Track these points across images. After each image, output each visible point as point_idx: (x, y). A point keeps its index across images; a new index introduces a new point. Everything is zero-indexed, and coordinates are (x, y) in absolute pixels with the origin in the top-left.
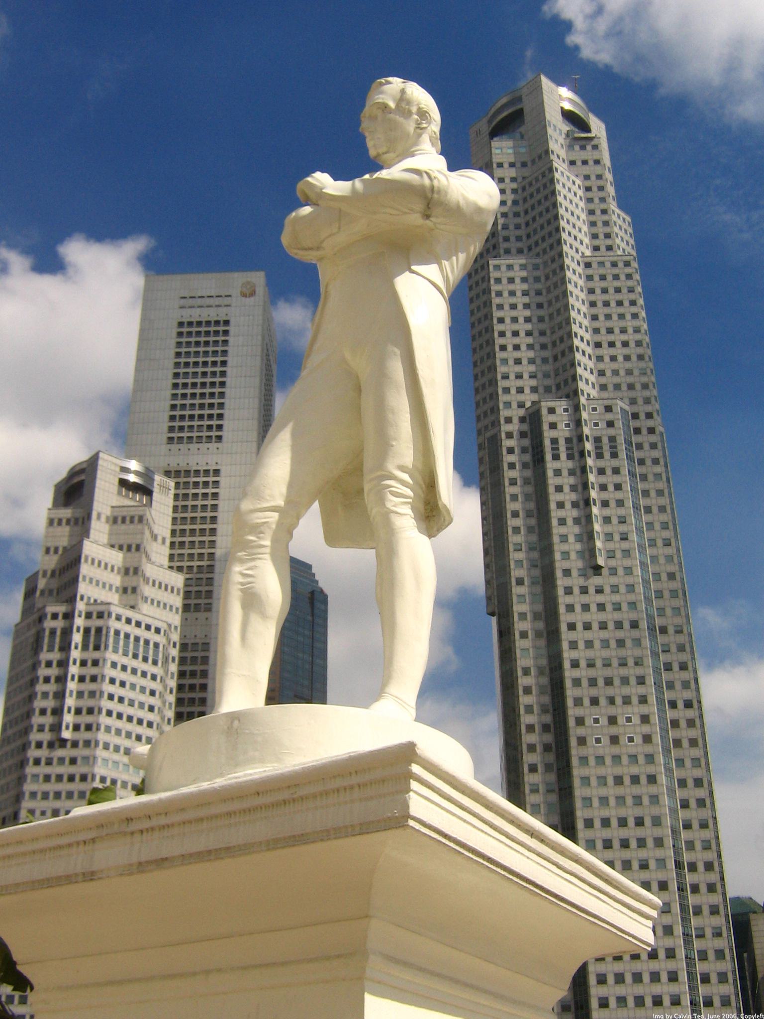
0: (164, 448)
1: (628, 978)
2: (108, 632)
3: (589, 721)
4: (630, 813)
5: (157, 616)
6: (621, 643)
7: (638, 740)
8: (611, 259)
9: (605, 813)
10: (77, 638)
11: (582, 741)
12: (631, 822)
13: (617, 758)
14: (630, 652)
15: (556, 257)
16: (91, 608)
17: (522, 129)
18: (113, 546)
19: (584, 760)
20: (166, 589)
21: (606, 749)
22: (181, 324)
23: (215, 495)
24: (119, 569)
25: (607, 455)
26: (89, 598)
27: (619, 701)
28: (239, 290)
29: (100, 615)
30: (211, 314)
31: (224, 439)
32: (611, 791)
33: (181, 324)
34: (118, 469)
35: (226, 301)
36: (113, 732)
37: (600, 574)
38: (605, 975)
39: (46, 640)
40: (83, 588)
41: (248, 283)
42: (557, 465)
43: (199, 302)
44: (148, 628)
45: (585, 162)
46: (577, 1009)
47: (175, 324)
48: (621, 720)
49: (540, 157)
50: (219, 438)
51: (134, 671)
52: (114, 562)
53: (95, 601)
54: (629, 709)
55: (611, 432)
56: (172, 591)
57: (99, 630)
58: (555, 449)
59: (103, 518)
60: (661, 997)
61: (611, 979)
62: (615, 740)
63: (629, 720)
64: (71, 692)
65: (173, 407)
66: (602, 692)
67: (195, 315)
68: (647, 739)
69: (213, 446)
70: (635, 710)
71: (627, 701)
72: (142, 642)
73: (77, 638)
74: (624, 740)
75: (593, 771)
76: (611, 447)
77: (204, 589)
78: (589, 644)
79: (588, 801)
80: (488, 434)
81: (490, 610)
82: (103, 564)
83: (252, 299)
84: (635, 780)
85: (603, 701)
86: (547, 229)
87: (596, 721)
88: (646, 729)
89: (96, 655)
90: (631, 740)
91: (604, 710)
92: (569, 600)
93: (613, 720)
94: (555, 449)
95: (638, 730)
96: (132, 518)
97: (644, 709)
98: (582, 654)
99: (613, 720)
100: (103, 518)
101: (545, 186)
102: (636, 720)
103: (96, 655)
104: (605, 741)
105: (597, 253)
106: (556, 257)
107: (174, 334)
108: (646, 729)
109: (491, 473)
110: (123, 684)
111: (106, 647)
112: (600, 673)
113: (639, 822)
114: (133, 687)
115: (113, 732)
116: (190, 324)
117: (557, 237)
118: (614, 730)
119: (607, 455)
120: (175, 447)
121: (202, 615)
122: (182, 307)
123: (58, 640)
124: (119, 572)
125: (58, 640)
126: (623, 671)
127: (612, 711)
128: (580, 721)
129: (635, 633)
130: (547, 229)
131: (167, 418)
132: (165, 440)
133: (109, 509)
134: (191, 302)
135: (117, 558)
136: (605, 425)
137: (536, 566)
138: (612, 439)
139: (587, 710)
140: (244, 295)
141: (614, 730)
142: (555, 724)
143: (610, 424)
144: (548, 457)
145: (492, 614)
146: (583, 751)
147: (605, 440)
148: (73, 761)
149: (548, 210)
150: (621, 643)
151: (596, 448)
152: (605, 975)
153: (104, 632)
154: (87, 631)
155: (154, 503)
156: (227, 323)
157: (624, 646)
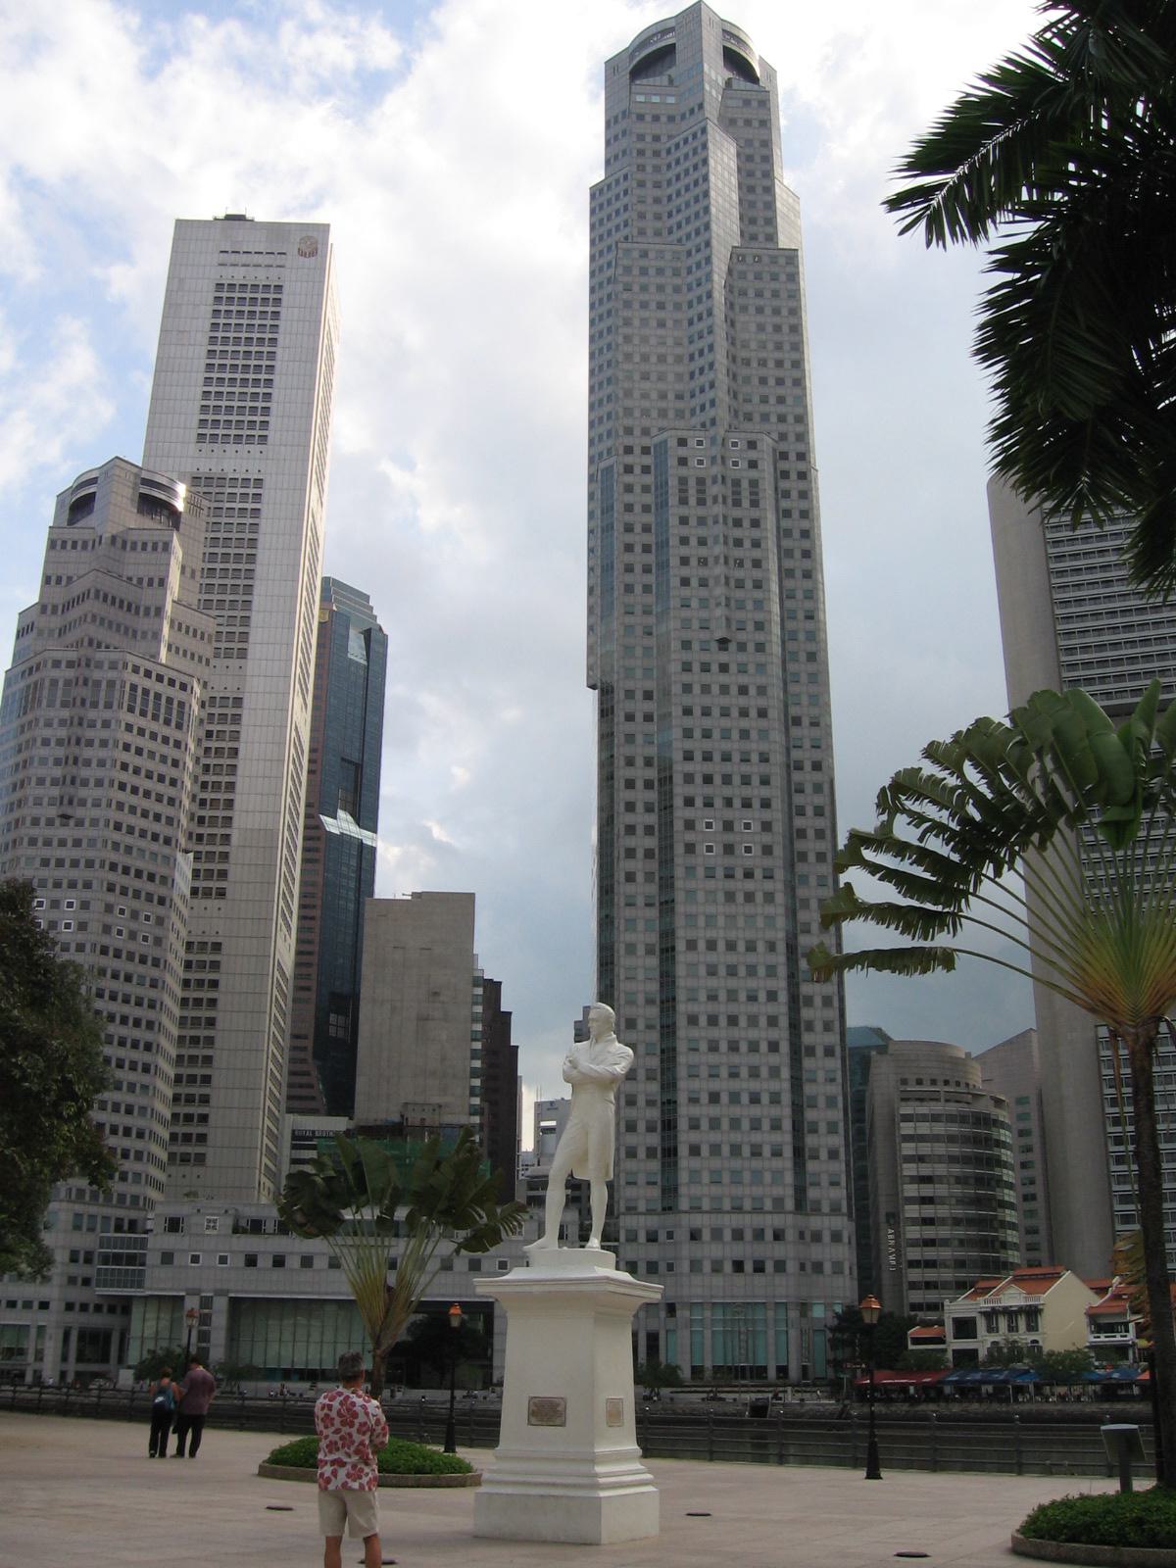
0: (193, 448)
1: (725, 1124)
2: (123, 686)
3: (701, 826)
5: (183, 669)
6: (745, 734)
7: (757, 850)
8: (771, 252)
9: (711, 934)
11: (690, 848)
14: (754, 746)
15: (703, 246)
17: (673, 72)
19: (690, 870)
20: (195, 635)
22: (219, 286)
27: (737, 803)
28: (296, 247)
30: (261, 277)
31: (270, 440)
33: (219, 286)
35: (280, 260)
36: (126, 809)
37: (726, 649)
38: (698, 1120)
39: (45, 693)
41: (309, 238)
42: (684, 511)
43: (244, 259)
44: (172, 682)
45: (748, 122)
46: (663, 1129)
47: (212, 287)
49: (692, 111)
50: (263, 439)
51: (154, 736)
54: (747, 812)
55: (754, 474)
56: (202, 638)
58: (683, 491)
60: (758, 1094)
61: (705, 1124)
66: (718, 791)
67: (238, 275)
68: (767, 850)
69: (255, 448)
70: (756, 814)
71: (747, 804)
72: (163, 701)
74: (740, 850)
76: (751, 494)
77: (238, 630)
78: (706, 689)
79: (691, 918)
80: (603, 465)
81: (592, 682)
84: (754, 1047)
86: (694, 208)
88: (767, 838)
90: (748, 850)
91: (720, 812)
93: (728, 826)
94: (683, 491)
95: (757, 838)
97: (767, 815)
98: (724, 1033)
99: (728, 826)
101: (695, 152)
102: (756, 827)
104: (718, 849)
106: (703, 246)
107: (211, 300)
108: (767, 838)
109: (602, 513)
110: (139, 751)
111: (120, 706)
112: (716, 768)
114: (152, 755)
115: (126, 809)
117: (704, 172)
118: (729, 838)
121: (234, 663)
123: (60, 693)
125: (60, 693)
126: (745, 768)
128: (690, 825)
129: (762, 723)
130: (694, 208)
131: (197, 409)
132: (194, 437)
134: (233, 258)
136: (746, 465)
138: (754, 484)
139: (696, 813)
140: (302, 253)
141: (729, 838)
142: (660, 825)
143: (753, 464)
144: (673, 500)
145: (593, 687)
146: (691, 860)
147: (745, 484)
148: (77, 843)
149: (696, 183)
150: (745, 734)
151: (734, 493)
152: (698, 1120)
153: (118, 686)
156: (279, 288)
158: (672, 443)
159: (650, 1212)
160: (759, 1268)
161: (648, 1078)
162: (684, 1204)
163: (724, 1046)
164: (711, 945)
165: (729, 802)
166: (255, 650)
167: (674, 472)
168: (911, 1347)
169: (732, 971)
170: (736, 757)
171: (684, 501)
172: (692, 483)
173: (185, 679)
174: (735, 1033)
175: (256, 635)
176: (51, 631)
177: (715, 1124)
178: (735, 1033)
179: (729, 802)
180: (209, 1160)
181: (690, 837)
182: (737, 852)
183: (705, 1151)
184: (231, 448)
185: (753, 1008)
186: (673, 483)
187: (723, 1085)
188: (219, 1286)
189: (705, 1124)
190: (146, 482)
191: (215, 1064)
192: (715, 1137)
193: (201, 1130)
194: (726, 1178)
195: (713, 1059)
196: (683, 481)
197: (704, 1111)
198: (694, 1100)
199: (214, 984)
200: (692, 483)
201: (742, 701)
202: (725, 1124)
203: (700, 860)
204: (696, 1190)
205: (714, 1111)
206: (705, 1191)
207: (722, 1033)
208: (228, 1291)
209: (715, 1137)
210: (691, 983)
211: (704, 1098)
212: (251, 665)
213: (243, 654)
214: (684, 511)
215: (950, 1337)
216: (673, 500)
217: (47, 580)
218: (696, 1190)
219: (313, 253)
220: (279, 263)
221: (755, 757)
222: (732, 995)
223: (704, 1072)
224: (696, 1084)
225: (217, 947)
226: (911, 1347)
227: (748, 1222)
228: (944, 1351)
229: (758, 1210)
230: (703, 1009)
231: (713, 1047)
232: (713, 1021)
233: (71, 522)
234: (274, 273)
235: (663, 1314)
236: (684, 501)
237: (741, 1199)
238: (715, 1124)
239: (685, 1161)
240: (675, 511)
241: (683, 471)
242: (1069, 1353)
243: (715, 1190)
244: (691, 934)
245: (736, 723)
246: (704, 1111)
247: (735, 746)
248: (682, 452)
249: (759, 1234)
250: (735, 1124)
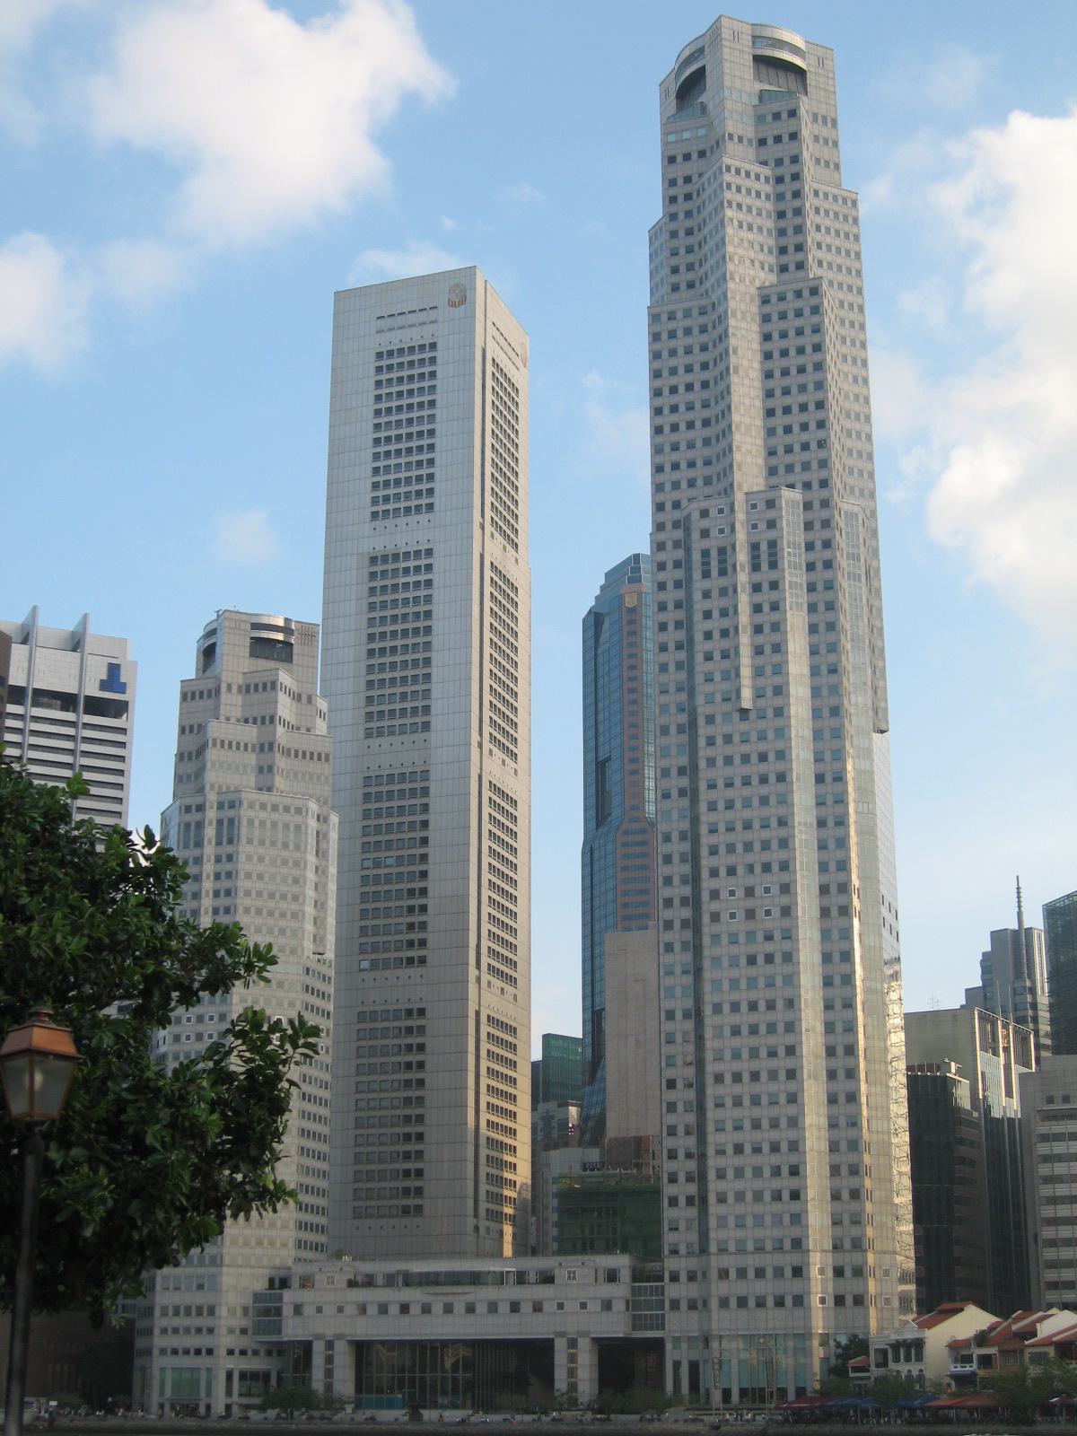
1: (748, 1173)
4: (761, 996)
6: (764, 801)
10: (210, 832)
11: (715, 917)
12: (762, 1006)
13: (751, 935)
16: (223, 798)
18: (246, 721)
19: (716, 938)
21: (740, 925)
22: (379, 355)
23: (429, 583)
24: (253, 746)
25: (765, 566)
26: (220, 786)
29: (232, 806)
30: (415, 337)
32: (744, 971)
33: (379, 355)
34: (249, 627)
40: (211, 776)
41: (457, 285)
42: (706, 584)
43: (400, 320)
47: (373, 357)
48: (759, 891)
50: (430, 507)
52: (246, 739)
53: (228, 787)
54: (767, 877)
57: (231, 821)
58: (706, 564)
59: (235, 689)
62: (750, 914)
63: (767, 890)
64: (207, 892)
65: (376, 471)
66: (740, 859)
67: (395, 340)
69: (423, 517)
73: (210, 832)
75: (724, 950)
82: (226, 745)
83: (462, 307)
85: (741, 870)
87: (732, 893)
89: (230, 849)
92: (710, 752)
93: (750, 892)
94: (706, 564)
96: (256, 689)
99: (750, 892)
100: (235, 689)
102: (775, 890)
103: (230, 849)
105: (785, 276)
113: (771, 1006)
116: (390, 353)
119: (765, 566)
120: (380, 523)
122: (379, 332)
124: (253, 750)
127: (749, 881)
133: (241, 676)
134: (390, 322)
135: (250, 733)
137: (683, 710)
140: (452, 304)
144: (697, 575)
146: (716, 928)
154: (220, 822)
155: (295, 657)
157: (768, 804)
158: (695, 516)
159: (690, 1254)
160: (780, 1303)
161: (687, 1133)
162: (713, 1248)
163: (746, 1101)
164: (735, 1007)
165: (751, 869)
166: (437, 721)
167: (698, 544)
168: (851, 1375)
169: (754, 1030)
170: (756, 824)
171: (706, 574)
172: (714, 554)
173: (299, 803)
174: (757, 1088)
175: (437, 706)
176: (189, 777)
177: (739, 1173)
178: (757, 1088)
179: (751, 869)
180: (426, 1211)
181: (715, 906)
182: (758, 917)
183: (731, 1198)
184: (402, 521)
185: (772, 1063)
186: (696, 557)
187: (747, 1137)
188: (559, 1330)
189: (730, 1174)
190: (256, 626)
191: (427, 1121)
192: (739, 1185)
193: (417, 1183)
194: (749, 1221)
195: (737, 1113)
196: (705, 554)
197: (731, 1161)
198: (721, 1152)
199: (421, 1048)
200: (714, 554)
201: (763, 768)
202: (748, 1173)
203: (724, 927)
204: (723, 1234)
205: (739, 1161)
206: (731, 1235)
207: (745, 1089)
208: (590, 1332)
209: (739, 1185)
210: (717, 1044)
211: (730, 1150)
212: (434, 737)
213: (426, 726)
214: (706, 584)
215: (873, 1368)
216: (697, 575)
217: (182, 730)
218: (723, 1234)
219: (463, 301)
220: (432, 318)
221: (774, 823)
222: (754, 1053)
223: (729, 1126)
224: (721, 1137)
225: (422, 1012)
226: (851, 1375)
227: (753, 1261)
228: (869, 1378)
229: (741, 1251)
230: (727, 1067)
231: (738, 1102)
232: (737, 1078)
233: (204, 671)
234: (429, 329)
235: (701, 1345)
236: (706, 574)
237: (763, 1240)
238: (739, 1173)
239: (714, 1209)
240: (699, 584)
241: (705, 544)
242: (596, 1356)
243: (740, 1233)
244: (717, 998)
245: (756, 790)
246: (731, 1161)
247: (755, 814)
248: (705, 523)
249: (742, 1273)
250: (757, 1172)
